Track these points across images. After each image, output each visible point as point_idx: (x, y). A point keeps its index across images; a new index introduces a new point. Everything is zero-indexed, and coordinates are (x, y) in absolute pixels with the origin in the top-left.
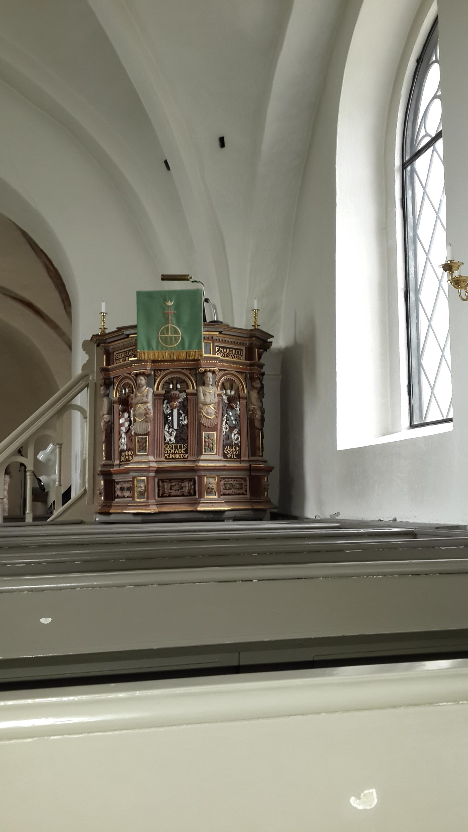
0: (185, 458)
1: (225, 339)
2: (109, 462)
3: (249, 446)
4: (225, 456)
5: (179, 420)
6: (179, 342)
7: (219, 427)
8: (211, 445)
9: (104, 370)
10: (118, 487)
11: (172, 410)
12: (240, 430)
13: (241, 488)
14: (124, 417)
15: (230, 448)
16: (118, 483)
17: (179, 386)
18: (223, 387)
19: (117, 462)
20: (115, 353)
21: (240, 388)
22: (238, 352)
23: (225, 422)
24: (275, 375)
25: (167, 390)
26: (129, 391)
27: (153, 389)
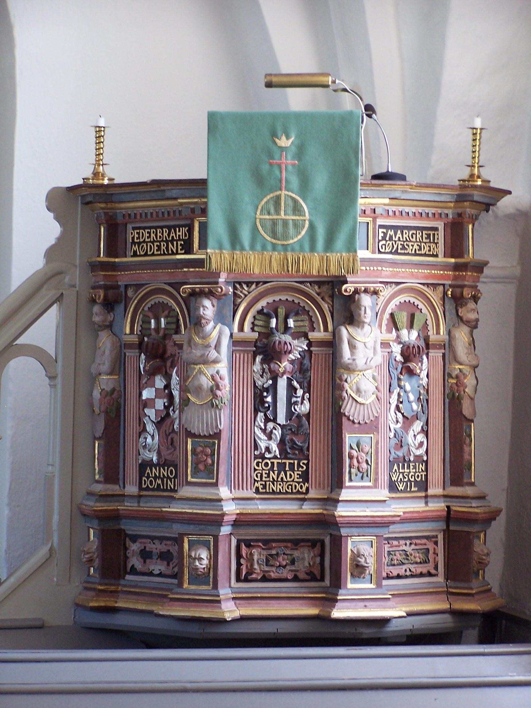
0: (302, 493)
1: (400, 209)
3: (447, 460)
4: (393, 487)
5: (290, 404)
6: (303, 233)
7: (381, 420)
8: (364, 465)
10: (135, 547)
11: (275, 379)
13: (426, 562)
14: (153, 386)
16: (134, 538)
17: (291, 323)
19: (132, 489)
20: (130, 227)
21: (429, 322)
22: (428, 236)
25: (263, 330)
26: (167, 323)
27: (231, 329)
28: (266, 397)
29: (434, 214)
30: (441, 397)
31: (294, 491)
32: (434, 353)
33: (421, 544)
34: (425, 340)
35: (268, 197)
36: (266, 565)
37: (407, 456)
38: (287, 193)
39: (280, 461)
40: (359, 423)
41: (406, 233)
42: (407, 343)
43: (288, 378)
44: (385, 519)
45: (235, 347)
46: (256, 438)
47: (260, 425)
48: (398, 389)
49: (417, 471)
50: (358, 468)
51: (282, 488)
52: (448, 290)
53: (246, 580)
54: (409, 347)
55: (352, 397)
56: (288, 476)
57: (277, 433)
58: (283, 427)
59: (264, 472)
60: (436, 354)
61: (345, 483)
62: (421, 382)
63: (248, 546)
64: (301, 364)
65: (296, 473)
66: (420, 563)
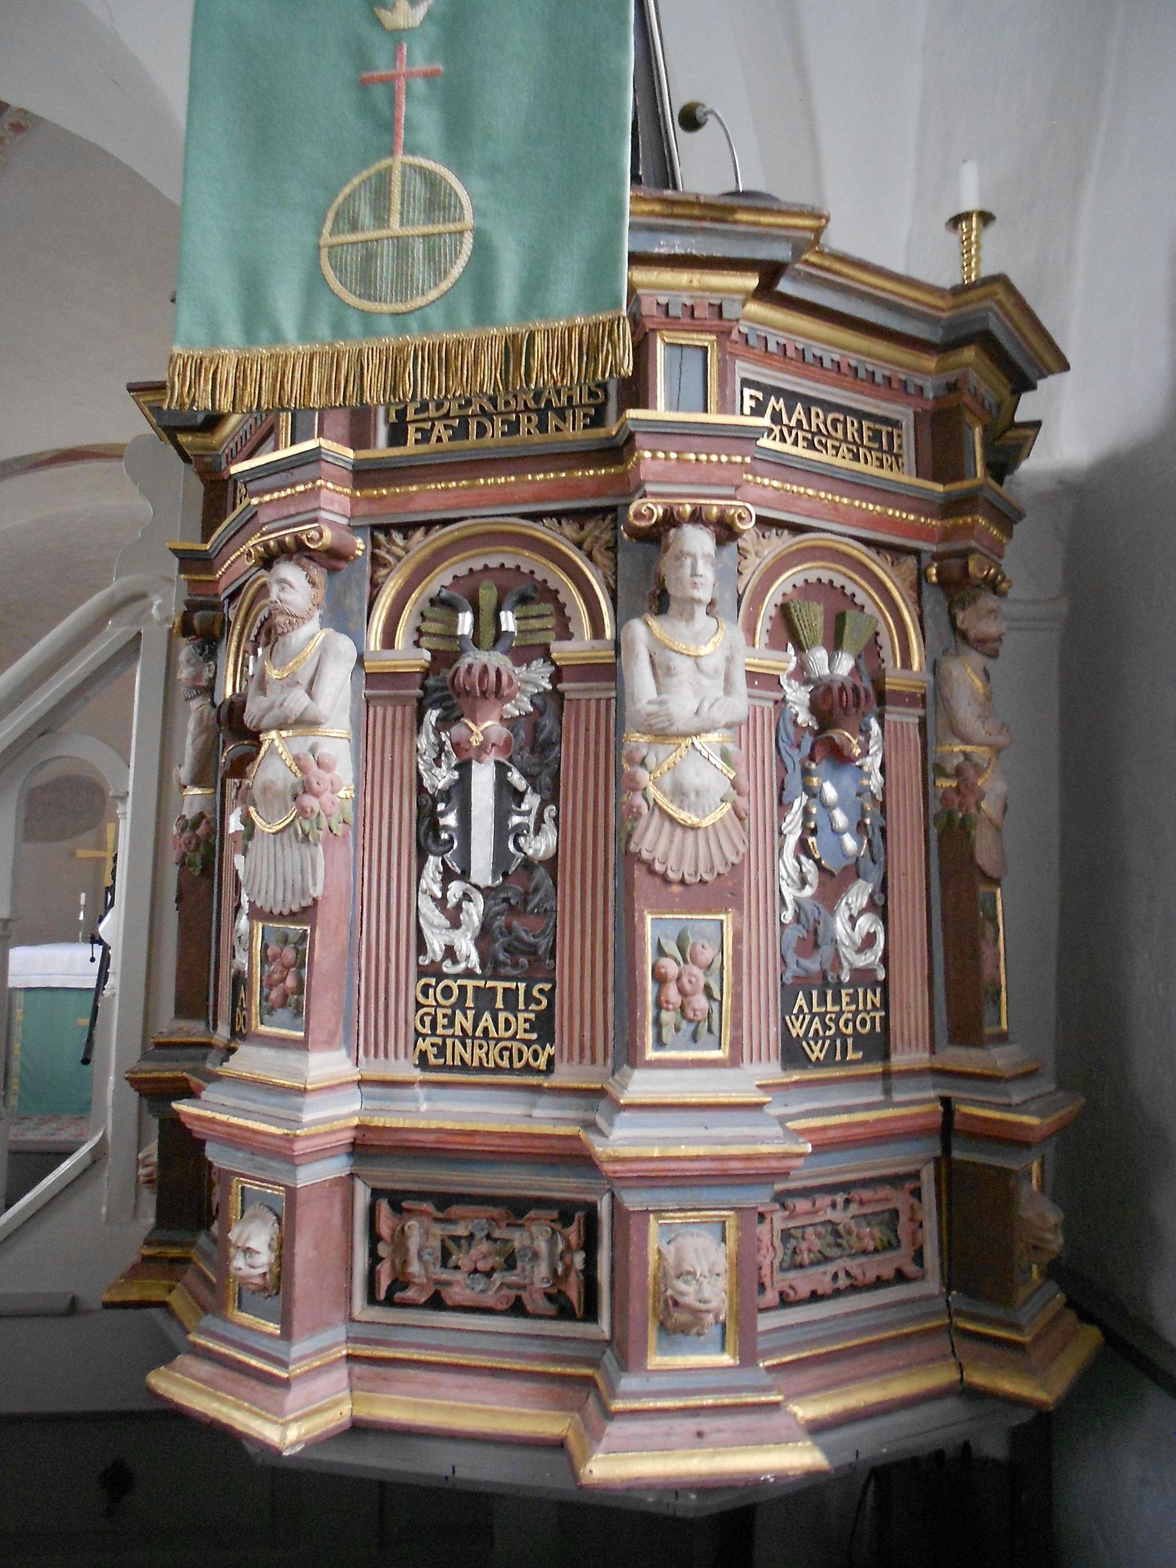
0: (539, 1072)
1: (801, 343)
2: (194, 1029)
3: (939, 980)
4: (792, 1053)
5: (501, 831)
6: (456, 271)
7: (755, 876)
9: (190, 561)
11: (464, 768)
12: (884, 887)
15: (822, 1001)
17: (509, 622)
18: (788, 627)
21: (883, 640)
22: (876, 436)
23: (792, 841)
24: (1035, 602)
25: (442, 645)
27: (358, 640)
28: (443, 814)
29: (888, 380)
30: (917, 821)
31: (517, 1065)
32: (899, 713)
33: (878, 1201)
34: (873, 682)
35: (356, 181)
36: (444, 1265)
37: (833, 970)
38: (410, 159)
39: (481, 983)
40: (682, 882)
41: (818, 415)
42: (825, 681)
43: (497, 763)
44: (758, 1164)
45: (372, 688)
46: (421, 920)
47: (431, 890)
48: (805, 797)
49: (861, 1007)
50: (682, 1008)
51: (487, 1054)
52: (930, 566)
53: (390, 1302)
54: (829, 689)
55: (660, 808)
56: (501, 1025)
57: (473, 911)
58: (486, 892)
59: (440, 1012)
60: (904, 718)
61: (644, 1054)
62: (865, 782)
63: (396, 1208)
64: (536, 728)
65: (521, 1016)
66: (876, 1251)
